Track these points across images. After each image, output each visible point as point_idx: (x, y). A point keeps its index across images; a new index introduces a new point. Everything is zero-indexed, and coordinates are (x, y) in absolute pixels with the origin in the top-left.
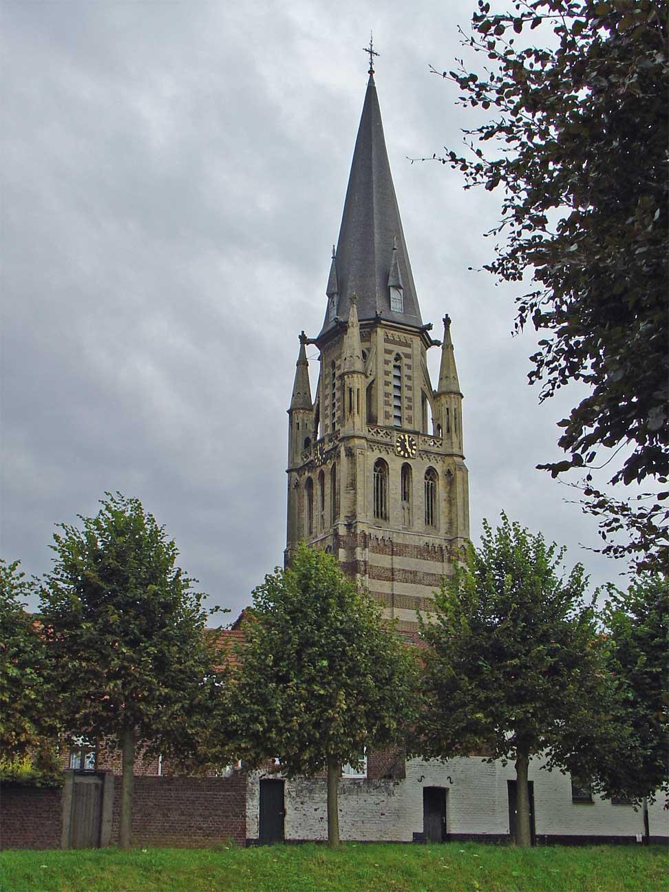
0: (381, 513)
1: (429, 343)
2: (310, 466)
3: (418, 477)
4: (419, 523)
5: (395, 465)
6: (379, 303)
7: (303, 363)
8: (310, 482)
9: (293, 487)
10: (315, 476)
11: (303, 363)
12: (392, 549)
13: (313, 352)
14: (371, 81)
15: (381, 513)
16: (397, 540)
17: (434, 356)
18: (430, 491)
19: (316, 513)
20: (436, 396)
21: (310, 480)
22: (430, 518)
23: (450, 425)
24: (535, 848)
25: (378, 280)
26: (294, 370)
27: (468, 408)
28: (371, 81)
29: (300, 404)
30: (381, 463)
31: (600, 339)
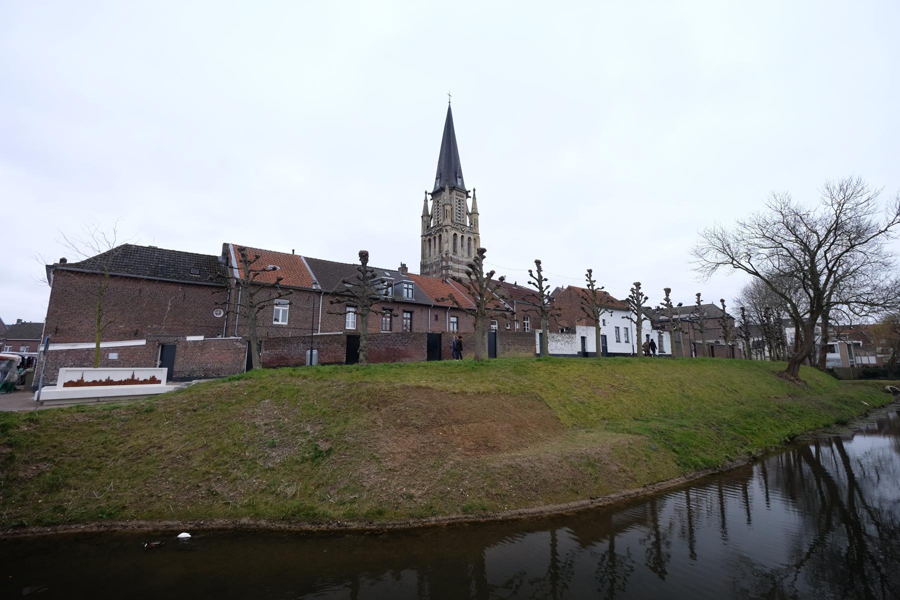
0: (455, 251)
1: (468, 197)
2: (430, 235)
3: (466, 239)
4: (466, 255)
5: (459, 235)
6: (454, 182)
7: (426, 201)
8: (430, 240)
9: (423, 242)
10: (432, 238)
11: (426, 201)
12: (459, 262)
13: (429, 197)
14: (449, 110)
15: (455, 251)
16: (460, 259)
17: (469, 202)
18: (469, 244)
19: (432, 250)
20: (470, 214)
21: (430, 240)
22: (469, 253)
23: (475, 224)
24: (777, 440)
25: (453, 174)
26: (423, 203)
27: (480, 219)
28: (449, 110)
29: (426, 216)
30: (455, 234)
31: (143, 342)
